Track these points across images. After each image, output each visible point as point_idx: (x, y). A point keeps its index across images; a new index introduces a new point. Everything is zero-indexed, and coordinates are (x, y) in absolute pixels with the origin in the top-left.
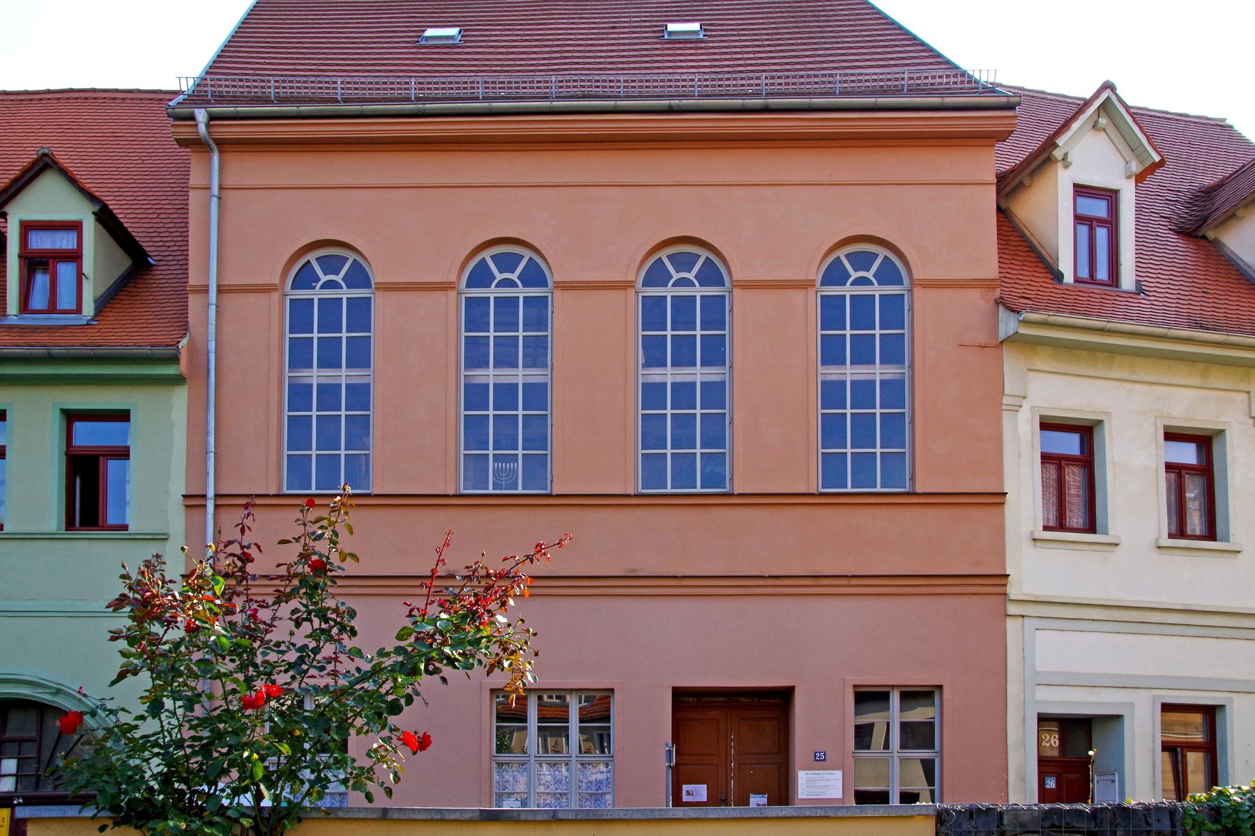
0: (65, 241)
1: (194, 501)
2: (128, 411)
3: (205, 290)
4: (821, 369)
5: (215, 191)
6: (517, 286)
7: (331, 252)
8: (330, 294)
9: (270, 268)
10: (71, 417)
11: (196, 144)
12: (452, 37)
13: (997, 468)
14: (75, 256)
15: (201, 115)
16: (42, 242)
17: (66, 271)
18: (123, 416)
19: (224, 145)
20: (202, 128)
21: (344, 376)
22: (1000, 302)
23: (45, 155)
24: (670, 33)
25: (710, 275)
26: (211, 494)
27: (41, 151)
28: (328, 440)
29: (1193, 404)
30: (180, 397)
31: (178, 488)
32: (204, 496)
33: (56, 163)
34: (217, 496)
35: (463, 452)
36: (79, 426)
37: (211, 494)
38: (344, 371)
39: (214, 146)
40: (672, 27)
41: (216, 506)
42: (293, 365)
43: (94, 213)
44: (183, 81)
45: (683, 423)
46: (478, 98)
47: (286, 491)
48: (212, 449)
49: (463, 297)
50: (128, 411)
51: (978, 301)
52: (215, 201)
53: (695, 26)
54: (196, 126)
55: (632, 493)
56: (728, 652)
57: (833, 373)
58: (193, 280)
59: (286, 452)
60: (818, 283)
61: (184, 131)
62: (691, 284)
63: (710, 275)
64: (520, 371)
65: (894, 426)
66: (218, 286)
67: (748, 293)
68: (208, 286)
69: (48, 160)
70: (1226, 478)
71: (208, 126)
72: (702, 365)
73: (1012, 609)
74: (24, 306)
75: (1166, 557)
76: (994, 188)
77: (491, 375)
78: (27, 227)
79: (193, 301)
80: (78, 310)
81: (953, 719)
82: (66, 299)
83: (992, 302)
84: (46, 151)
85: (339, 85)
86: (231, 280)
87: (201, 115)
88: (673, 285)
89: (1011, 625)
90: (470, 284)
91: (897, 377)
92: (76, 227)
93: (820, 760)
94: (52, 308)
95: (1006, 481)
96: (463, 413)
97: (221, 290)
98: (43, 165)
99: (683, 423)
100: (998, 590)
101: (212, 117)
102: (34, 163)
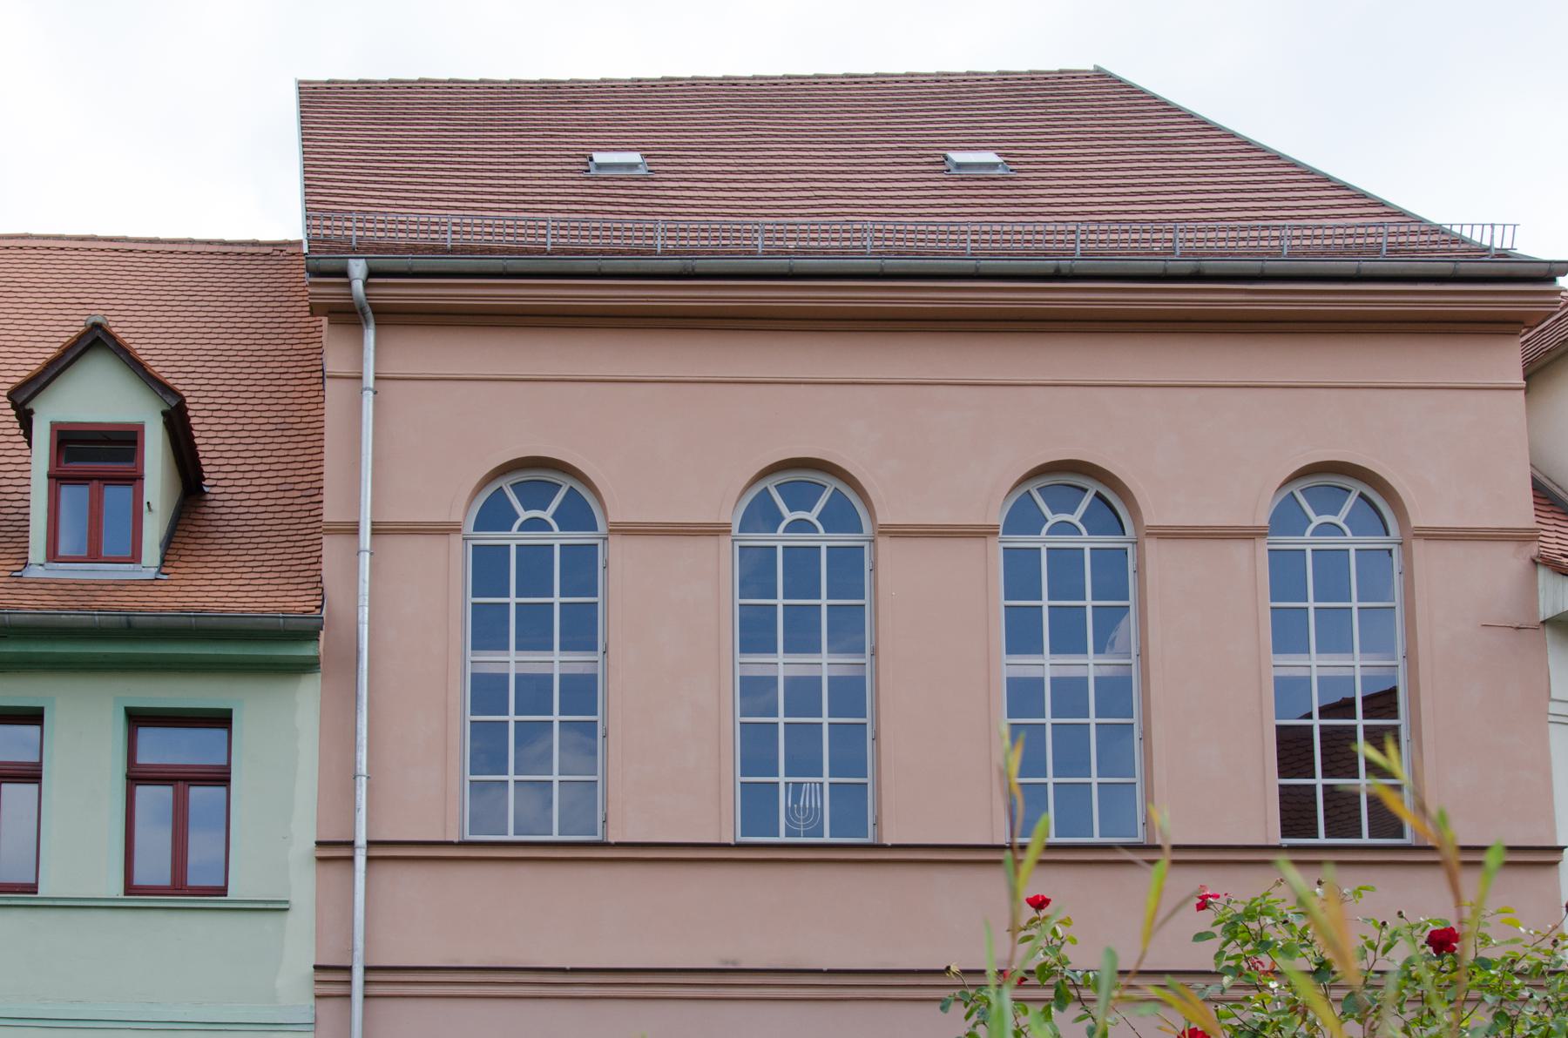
2: (230, 711)
3: (353, 530)
4: (1006, 659)
5: (369, 380)
6: (816, 531)
7: (536, 475)
8: (535, 538)
9: (454, 500)
10: (137, 719)
11: (347, 316)
12: (633, 166)
15: (358, 268)
18: (221, 720)
19: (391, 317)
20: (358, 286)
21: (557, 662)
22: (1543, 562)
23: (97, 326)
24: (600, 166)
25: (577, 514)
26: (361, 840)
27: (92, 320)
28: (1073, 760)
30: (307, 694)
32: (351, 844)
33: (113, 337)
34: (370, 844)
36: (146, 735)
37: (361, 840)
38: (825, 657)
39: (370, 315)
40: (599, 158)
41: (369, 859)
42: (1280, 646)
43: (164, 413)
45: (802, 737)
46: (755, 253)
47: (469, 837)
48: (363, 768)
49: (470, 543)
50: (230, 711)
51: (1510, 561)
52: (368, 398)
53: (990, 157)
54: (349, 285)
55: (456, 840)
57: (758, 664)
58: (331, 512)
59: (1138, 779)
60: (735, 529)
61: (329, 292)
62: (1337, 530)
63: (840, 517)
64: (557, 655)
65: (1116, 739)
66: (373, 523)
67: (1435, 546)
68: (357, 523)
69: (99, 333)
71: (366, 285)
72: (562, 649)
74: (53, 555)
77: (557, 662)
79: (332, 548)
80: (136, 557)
83: (1527, 561)
84: (99, 320)
85: (660, 234)
86: (392, 515)
87: (358, 268)
88: (1314, 533)
90: (478, 526)
91: (1121, 672)
95: (1559, 827)
98: (96, 340)
99: (802, 737)
101: (372, 273)
102: (81, 337)
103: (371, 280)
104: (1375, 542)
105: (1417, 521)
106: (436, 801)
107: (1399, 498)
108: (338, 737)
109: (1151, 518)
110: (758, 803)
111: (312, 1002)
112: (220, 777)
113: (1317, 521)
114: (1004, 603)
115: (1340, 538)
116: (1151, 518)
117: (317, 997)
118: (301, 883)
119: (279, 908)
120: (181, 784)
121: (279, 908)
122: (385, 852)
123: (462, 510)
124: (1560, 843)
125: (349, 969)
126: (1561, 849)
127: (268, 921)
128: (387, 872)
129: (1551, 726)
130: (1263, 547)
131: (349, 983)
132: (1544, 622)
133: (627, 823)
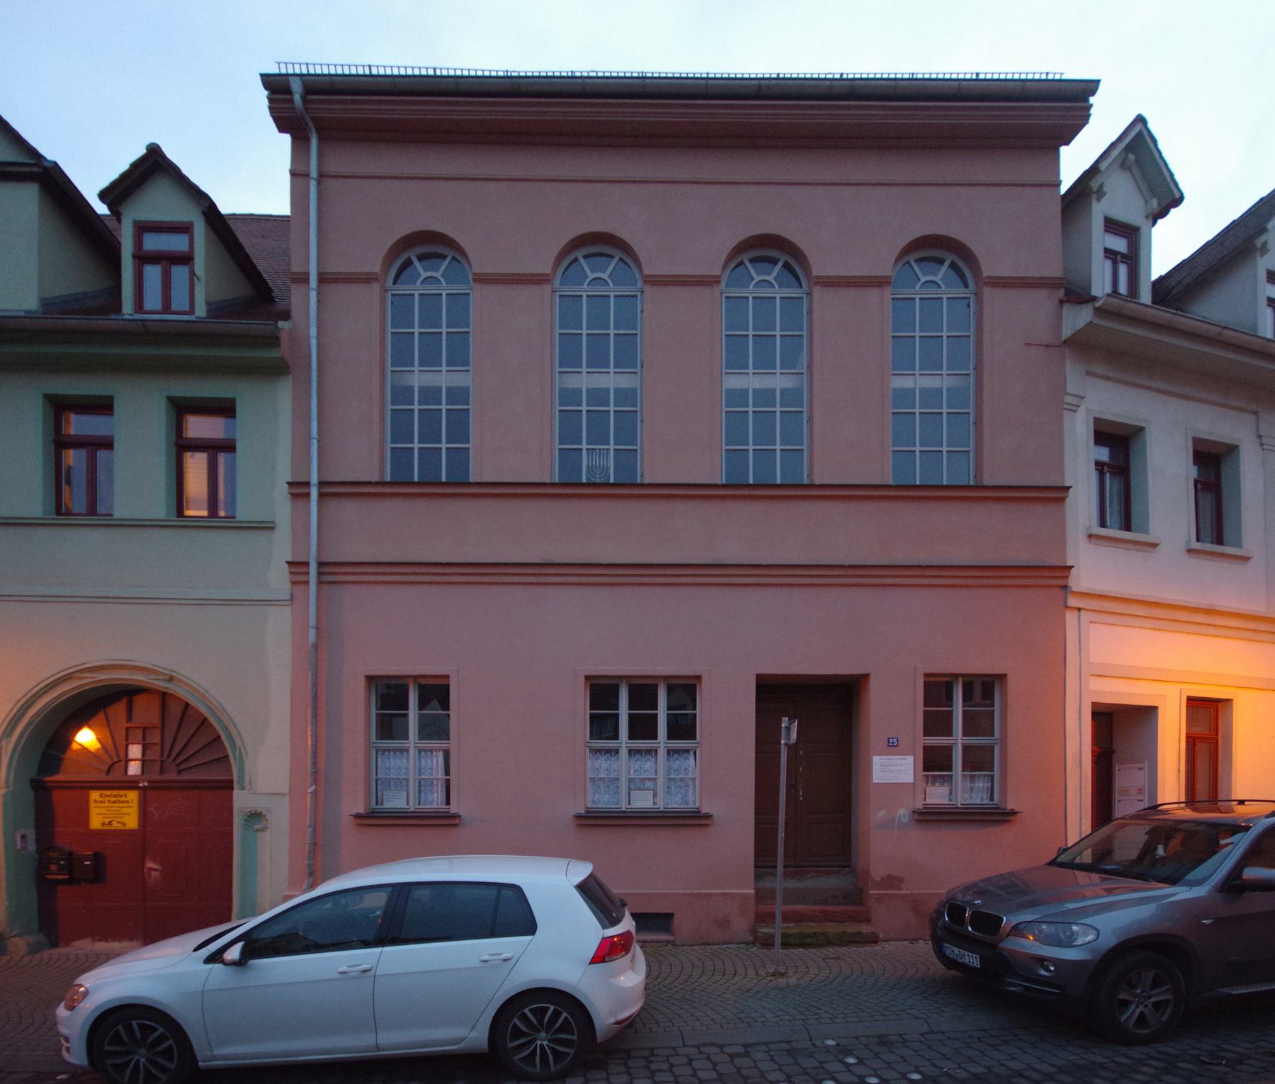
0: (177, 243)
1: (298, 489)
2: (111, 398)
8: (429, 289)
13: (201, 714)
14: (185, 259)
16: (153, 243)
17: (179, 273)
20: (297, 98)
29: (1220, 425)
30: (284, 393)
31: (284, 474)
32: (308, 484)
34: (321, 484)
35: (558, 446)
37: (314, 479)
44: (283, 66)
50: (111, 398)
54: (292, 101)
55: (548, 481)
56: (808, 640)
68: (308, 274)
70: (1239, 493)
71: (304, 100)
73: (1072, 602)
75: (1194, 561)
76: (286, 800)
78: (143, 228)
80: (192, 312)
81: (1016, 703)
82: (179, 300)
89: (1071, 618)
92: (185, 229)
93: (892, 746)
94: (167, 308)
96: (558, 408)
97: (323, 279)
100: (1061, 582)
103: (310, 97)
104: (793, 292)
105: (986, 272)
106: (364, 458)
107: (974, 256)
108: (301, 415)
109: (816, 271)
110: (569, 458)
111: (288, 586)
112: (108, 444)
113: (591, 276)
114: (470, 330)
115: (771, 290)
116: (816, 271)
117: (293, 583)
118: (281, 509)
119: (267, 527)
120: (90, 448)
121: (267, 527)
122: (332, 490)
123: (552, 260)
124: (1067, 484)
125: (307, 564)
126: (1069, 488)
127: (260, 537)
128: (333, 505)
129: (1066, 413)
130: (888, 293)
131: (308, 573)
132: (1065, 342)
133: (652, 470)
